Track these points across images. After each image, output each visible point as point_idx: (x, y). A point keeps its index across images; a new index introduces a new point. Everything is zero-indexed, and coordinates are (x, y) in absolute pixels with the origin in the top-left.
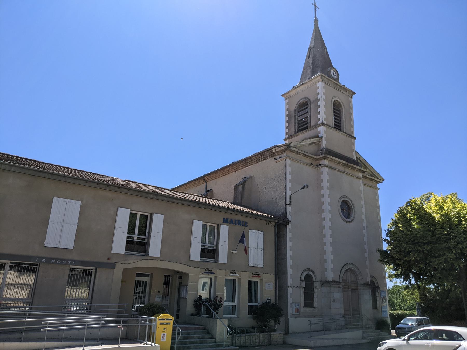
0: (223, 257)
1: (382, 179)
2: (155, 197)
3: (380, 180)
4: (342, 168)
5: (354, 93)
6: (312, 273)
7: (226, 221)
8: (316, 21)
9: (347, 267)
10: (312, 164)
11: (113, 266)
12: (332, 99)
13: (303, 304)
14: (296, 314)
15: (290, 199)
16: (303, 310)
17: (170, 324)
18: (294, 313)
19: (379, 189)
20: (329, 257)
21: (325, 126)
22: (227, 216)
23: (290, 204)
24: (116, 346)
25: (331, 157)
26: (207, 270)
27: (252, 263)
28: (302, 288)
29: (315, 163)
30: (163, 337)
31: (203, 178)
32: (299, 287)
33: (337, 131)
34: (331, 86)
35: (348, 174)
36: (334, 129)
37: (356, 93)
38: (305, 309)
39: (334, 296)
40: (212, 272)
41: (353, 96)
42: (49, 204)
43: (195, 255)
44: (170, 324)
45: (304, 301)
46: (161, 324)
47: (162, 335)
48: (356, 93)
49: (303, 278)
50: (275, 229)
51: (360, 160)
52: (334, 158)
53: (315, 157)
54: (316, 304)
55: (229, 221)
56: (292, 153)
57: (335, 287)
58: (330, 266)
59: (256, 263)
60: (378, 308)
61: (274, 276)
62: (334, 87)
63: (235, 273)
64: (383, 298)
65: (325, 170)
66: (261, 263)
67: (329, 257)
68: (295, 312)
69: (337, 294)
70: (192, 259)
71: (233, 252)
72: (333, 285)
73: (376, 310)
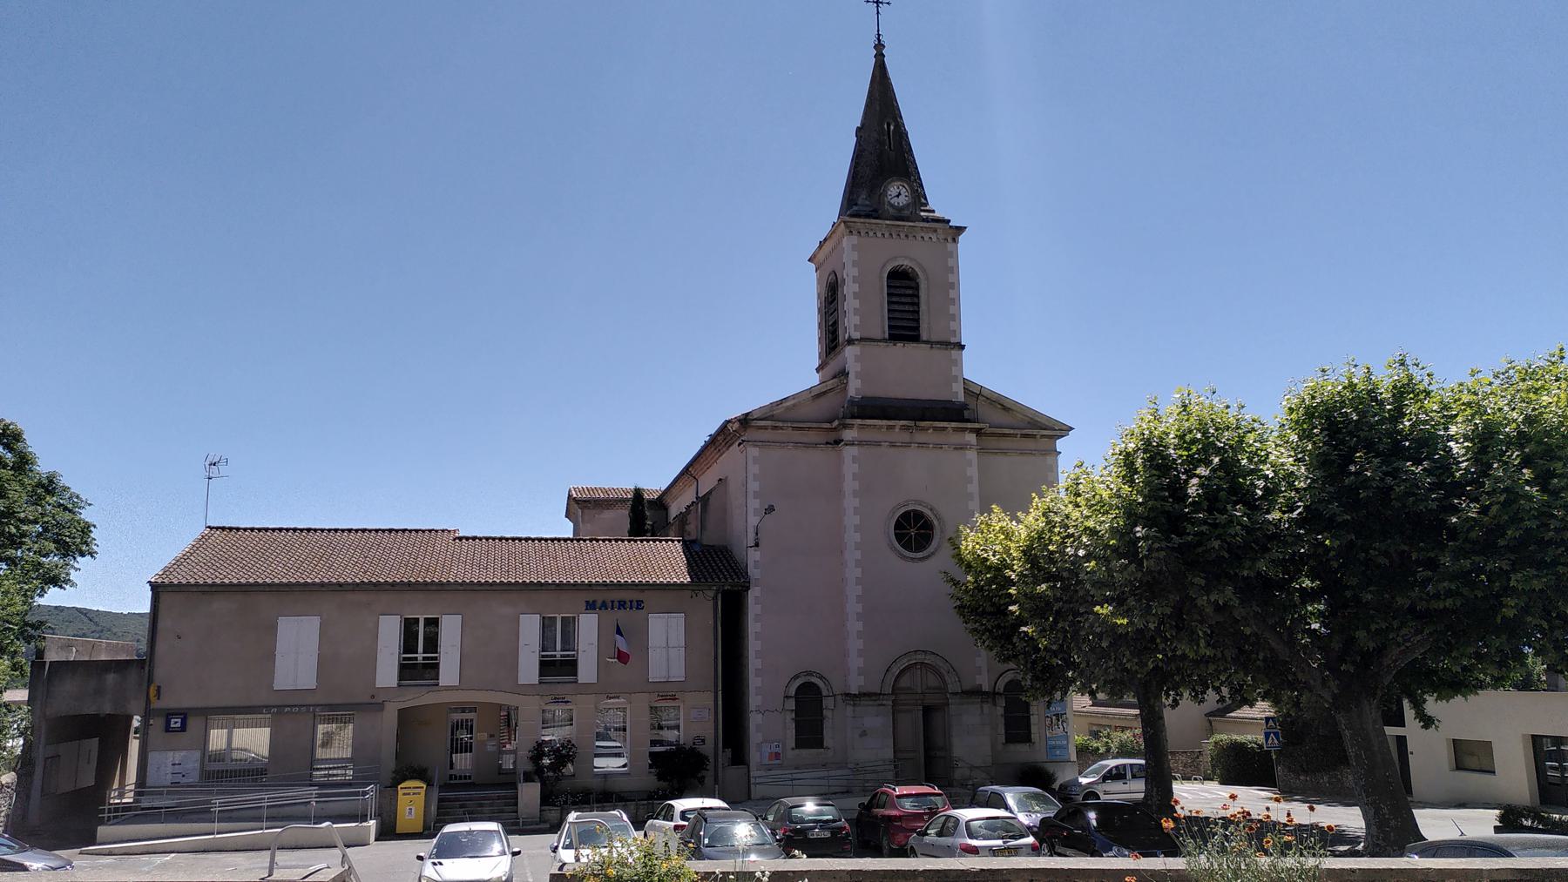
0: (587, 671)
1: (1065, 428)
2: (439, 588)
3: (1059, 430)
4: (905, 437)
5: (960, 230)
7: (591, 606)
8: (879, 46)
9: (909, 661)
11: (380, 707)
12: (883, 267)
14: (771, 762)
16: (791, 754)
17: (419, 794)
18: (766, 761)
19: (1060, 453)
20: (855, 644)
21: (854, 344)
23: (757, 545)
24: (354, 824)
25: (859, 421)
26: (555, 698)
28: (788, 713)
30: (410, 813)
31: (686, 471)
33: (895, 345)
34: (879, 235)
35: (921, 445)
38: (797, 751)
41: (961, 238)
42: (272, 629)
43: (529, 671)
44: (419, 794)
45: (794, 737)
46: (404, 794)
47: (408, 811)
48: (965, 228)
49: (792, 692)
51: (983, 396)
53: (827, 425)
54: (827, 742)
55: (598, 605)
58: (855, 662)
61: (713, 694)
62: (891, 234)
63: (618, 697)
65: (850, 452)
66: (678, 673)
67: (855, 644)
68: (770, 759)
69: (876, 719)
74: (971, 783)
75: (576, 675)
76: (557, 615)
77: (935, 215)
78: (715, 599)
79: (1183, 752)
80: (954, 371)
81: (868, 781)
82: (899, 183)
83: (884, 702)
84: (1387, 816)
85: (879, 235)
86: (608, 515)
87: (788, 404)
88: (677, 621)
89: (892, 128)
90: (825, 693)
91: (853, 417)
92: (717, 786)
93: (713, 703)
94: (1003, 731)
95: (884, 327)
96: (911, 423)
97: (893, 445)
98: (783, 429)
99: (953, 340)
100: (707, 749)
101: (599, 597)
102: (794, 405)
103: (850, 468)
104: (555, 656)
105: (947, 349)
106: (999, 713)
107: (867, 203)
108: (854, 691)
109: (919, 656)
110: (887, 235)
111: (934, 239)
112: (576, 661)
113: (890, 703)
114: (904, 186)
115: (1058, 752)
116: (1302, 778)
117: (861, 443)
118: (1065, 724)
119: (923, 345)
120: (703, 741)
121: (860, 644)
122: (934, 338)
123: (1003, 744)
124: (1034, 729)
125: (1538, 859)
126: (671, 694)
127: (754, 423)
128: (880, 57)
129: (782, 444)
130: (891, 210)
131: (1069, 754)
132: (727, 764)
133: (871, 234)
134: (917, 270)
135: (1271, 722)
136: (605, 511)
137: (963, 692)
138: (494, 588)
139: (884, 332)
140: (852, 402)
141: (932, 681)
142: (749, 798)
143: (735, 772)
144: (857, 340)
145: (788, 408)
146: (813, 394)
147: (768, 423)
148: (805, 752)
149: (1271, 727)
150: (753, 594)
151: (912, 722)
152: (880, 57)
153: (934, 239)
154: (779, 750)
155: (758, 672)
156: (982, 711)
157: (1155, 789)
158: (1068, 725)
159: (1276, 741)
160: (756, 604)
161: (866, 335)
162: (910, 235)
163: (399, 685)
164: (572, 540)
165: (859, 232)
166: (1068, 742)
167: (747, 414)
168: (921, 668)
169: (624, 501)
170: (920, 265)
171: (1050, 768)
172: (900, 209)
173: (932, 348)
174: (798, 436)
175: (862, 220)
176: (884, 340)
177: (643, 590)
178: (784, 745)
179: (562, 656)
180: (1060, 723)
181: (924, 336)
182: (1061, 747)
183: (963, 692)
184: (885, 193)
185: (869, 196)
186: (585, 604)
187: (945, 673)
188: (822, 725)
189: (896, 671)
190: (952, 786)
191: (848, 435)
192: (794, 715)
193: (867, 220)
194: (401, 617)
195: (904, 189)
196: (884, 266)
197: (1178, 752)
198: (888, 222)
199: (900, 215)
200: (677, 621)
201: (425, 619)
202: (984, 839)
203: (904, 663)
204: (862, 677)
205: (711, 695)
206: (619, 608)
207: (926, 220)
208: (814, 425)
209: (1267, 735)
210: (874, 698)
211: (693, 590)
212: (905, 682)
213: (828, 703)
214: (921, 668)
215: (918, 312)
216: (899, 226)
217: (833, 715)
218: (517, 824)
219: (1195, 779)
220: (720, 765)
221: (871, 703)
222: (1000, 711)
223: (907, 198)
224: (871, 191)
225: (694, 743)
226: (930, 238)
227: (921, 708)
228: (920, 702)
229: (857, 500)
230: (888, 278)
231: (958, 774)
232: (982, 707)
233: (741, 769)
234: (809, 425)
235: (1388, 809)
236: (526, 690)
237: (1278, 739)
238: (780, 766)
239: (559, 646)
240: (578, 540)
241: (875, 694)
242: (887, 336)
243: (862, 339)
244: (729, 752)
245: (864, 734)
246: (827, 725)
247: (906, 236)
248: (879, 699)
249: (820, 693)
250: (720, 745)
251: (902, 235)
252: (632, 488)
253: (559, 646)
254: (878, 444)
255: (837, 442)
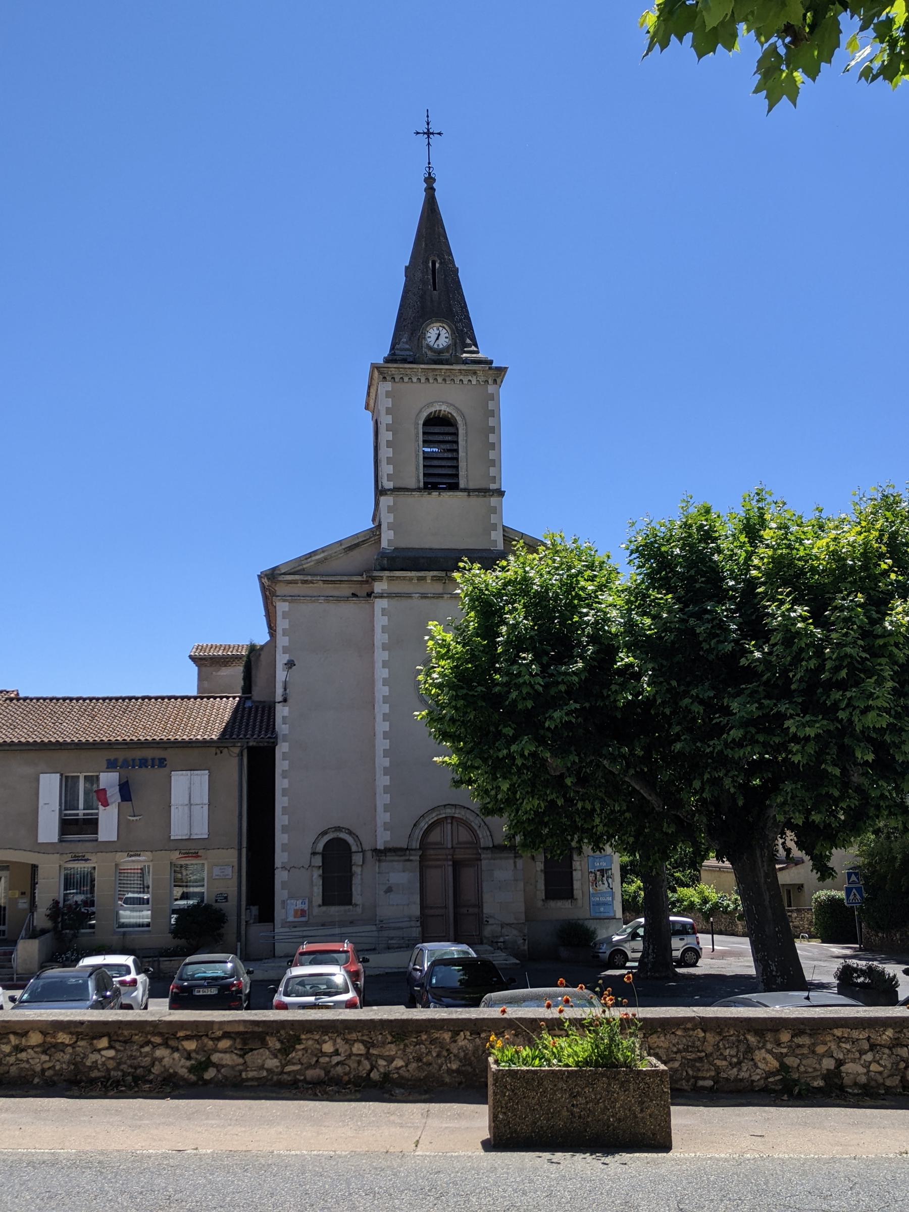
6: (348, 836)
8: (430, 180)
9: (437, 815)
10: (354, 595)
13: (318, 899)
14: (296, 920)
15: (285, 689)
16: (316, 911)
18: (291, 918)
22: (112, 755)
23: (285, 700)
25: (387, 573)
26: (75, 856)
27: (178, 831)
29: (362, 592)
32: (307, 867)
33: (429, 494)
34: (415, 380)
36: (418, 493)
37: (506, 368)
38: (324, 908)
39: (388, 880)
40: (86, 858)
49: (320, 847)
50: (241, 760)
52: (398, 574)
53: (360, 578)
54: (357, 898)
56: (295, 585)
57: (393, 861)
58: (383, 817)
59: (186, 831)
60: (575, 897)
62: (427, 379)
63: (139, 855)
64: (598, 873)
65: (381, 604)
66: (201, 830)
70: (41, 839)
71: (131, 818)
72: (388, 858)
73: (570, 901)
74: (502, 940)
75: (97, 834)
76: (79, 774)
77: (480, 355)
78: (241, 754)
79: (808, 910)
80: (494, 519)
81: (392, 938)
82: (438, 324)
83: (411, 858)
84: (774, 973)
85: (415, 380)
86: (225, 672)
87: (317, 557)
88: (201, 779)
89: (437, 265)
90: (354, 848)
91: (383, 569)
92: (239, 944)
93: (236, 860)
94: (543, 887)
95: (418, 477)
96: (443, 574)
97: (424, 596)
98: (313, 583)
99: (493, 486)
100: (230, 907)
101: (120, 755)
102: (326, 559)
103: (381, 621)
104: (77, 815)
105: (485, 497)
106: (538, 869)
107: (407, 346)
108: (380, 846)
109: (448, 811)
110: (423, 380)
111: (474, 382)
112: (97, 819)
113: (418, 858)
114: (444, 327)
115: (602, 909)
116: (880, 935)
117: (390, 596)
118: (610, 880)
119: (461, 493)
120: (226, 898)
121: (387, 798)
122: (471, 486)
123: (543, 900)
124: (577, 885)
125: (454, 1016)
126: (193, 851)
127: (281, 578)
128: (430, 191)
129: (313, 598)
130: (429, 353)
131: (615, 912)
132: (252, 921)
133: (406, 379)
134: (455, 415)
135: (853, 878)
136: (224, 668)
137: (494, 846)
138: (13, 748)
139: (419, 481)
140: (383, 555)
141: (464, 835)
142: (274, 956)
143: (258, 931)
144: (389, 490)
145: (319, 562)
146: (343, 547)
147: (297, 577)
148: (334, 910)
149: (854, 883)
150: (282, 749)
151: (441, 877)
152: (430, 191)
153: (474, 382)
154: (306, 907)
155: (285, 829)
156: (515, 866)
157: (651, 947)
158: (613, 881)
159: (858, 897)
160: (283, 760)
161: (398, 485)
162: (447, 379)
163: (61, 841)
164: (195, 698)
165: (393, 378)
166: (613, 899)
167: (274, 569)
168: (452, 823)
169: (237, 658)
170: (457, 409)
171: (591, 925)
172: (439, 352)
173: (469, 495)
174: (330, 590)
175: (395, 365)
176: (418, 489)
177: (166, 748)
178: (310, 902)
179: (84, 815)
180: (605, 879)
181: (462, 485)
182: (605, 904)
183: (494, 846)
184: (423, 337)
185: (410, 339)
186: (105, 762)
187: (476, 827)
188: (351, 881)
189: (424, 825)
190: (482, 943)
191: (379, 587)
192: (321, 871)
193: (401, 366)
194: (61, 775)
195: (444, 331)
196: (420, 411)
197: (804, 909)
198: (423, 366)
199: (439, 358)
200: (201, 779)
201: (85, 776)
202: (297, 996)
203: (433, 817)
204: (389, 833)
205: (234, 853)
206: (140, 767)
207: (465, 362)
208: (345, 578)
209: (848, 891)
210: (399, 853)
211: (218, 747)
212: (435, 837)
213: (357, 859)
214: (452, 823)
215: (457, 459)
216: (413, 368)
217: (362, 871)
218: (12, 979)
219: (803, 937)
220: (243, 923)
221: (397, 858)
222: (540, 866)
223: (447, 340)
224: (412, 334)
225: (216, 901)
226: (470, 381)
227: (451, 863)
228: (449, 857)
229: (387, 653)
230: (425, 424)
231: (487, 931)
232: (515, 863)
233: (267, 926)
234: (339, 578)
235: (775, 966)
236: (46, 848)
237: (861, 895)
238: (306, 924)
239: (81, 806)
240: (202, 698)
241: (401, 849)
242: (422, 485)
243: (396, 490)
244: (255, 910)
245: (389, 890)
246: (356, 881)
247: (444, 380)
248: (404, 855)
249: (350, 849)
250: (244, 903)
251: (440, 380)
252: (248, 643)
253: (81, 806)
254: (408, 596)
255: (369, 595)
